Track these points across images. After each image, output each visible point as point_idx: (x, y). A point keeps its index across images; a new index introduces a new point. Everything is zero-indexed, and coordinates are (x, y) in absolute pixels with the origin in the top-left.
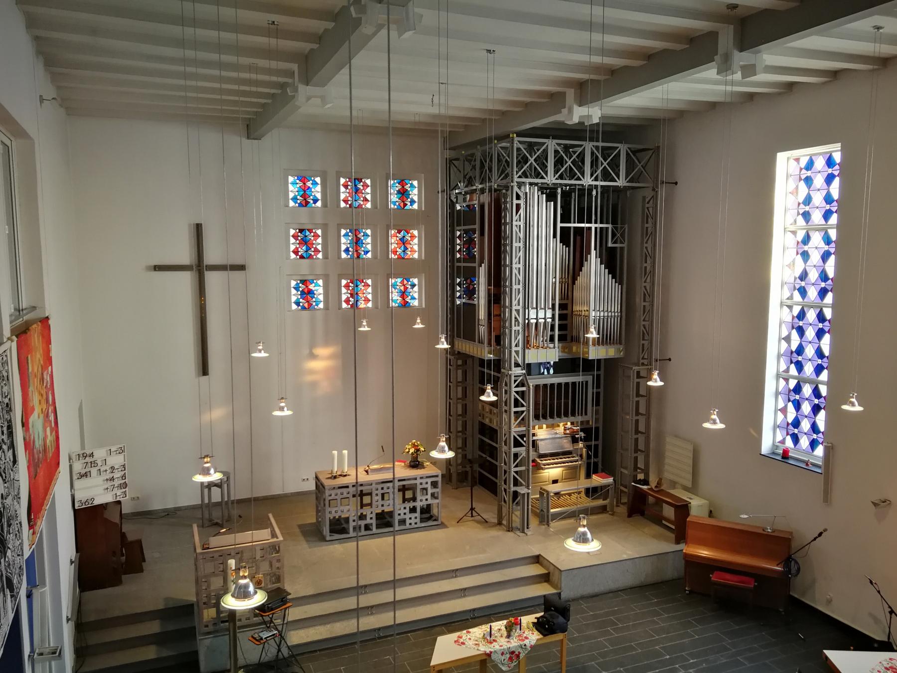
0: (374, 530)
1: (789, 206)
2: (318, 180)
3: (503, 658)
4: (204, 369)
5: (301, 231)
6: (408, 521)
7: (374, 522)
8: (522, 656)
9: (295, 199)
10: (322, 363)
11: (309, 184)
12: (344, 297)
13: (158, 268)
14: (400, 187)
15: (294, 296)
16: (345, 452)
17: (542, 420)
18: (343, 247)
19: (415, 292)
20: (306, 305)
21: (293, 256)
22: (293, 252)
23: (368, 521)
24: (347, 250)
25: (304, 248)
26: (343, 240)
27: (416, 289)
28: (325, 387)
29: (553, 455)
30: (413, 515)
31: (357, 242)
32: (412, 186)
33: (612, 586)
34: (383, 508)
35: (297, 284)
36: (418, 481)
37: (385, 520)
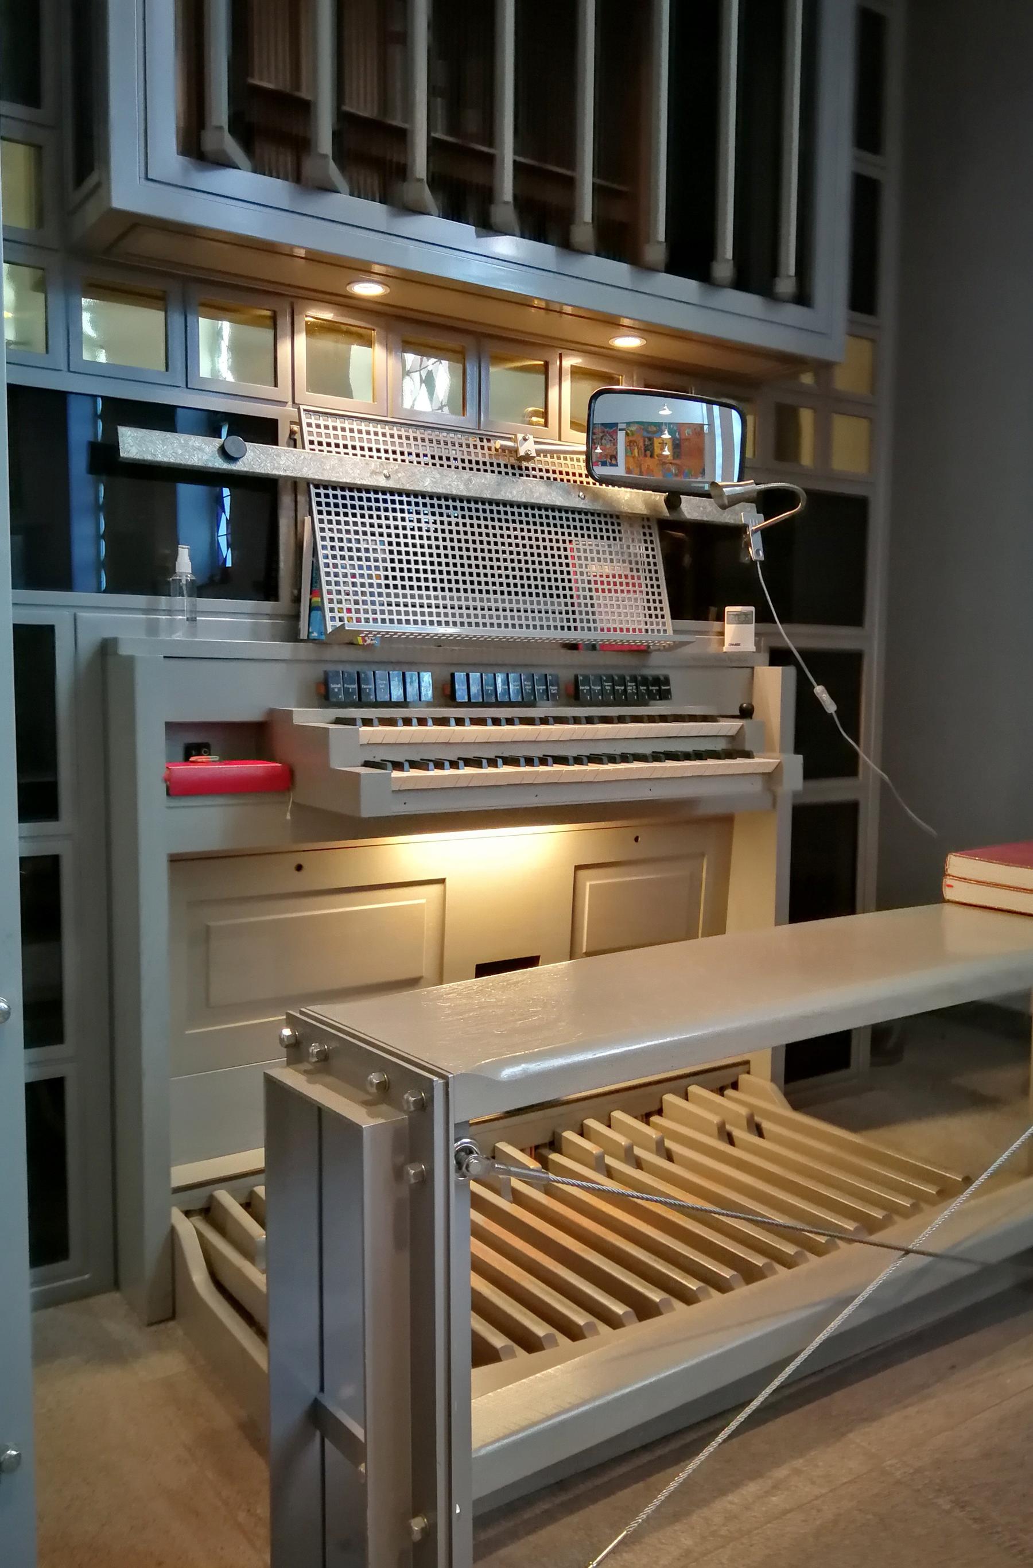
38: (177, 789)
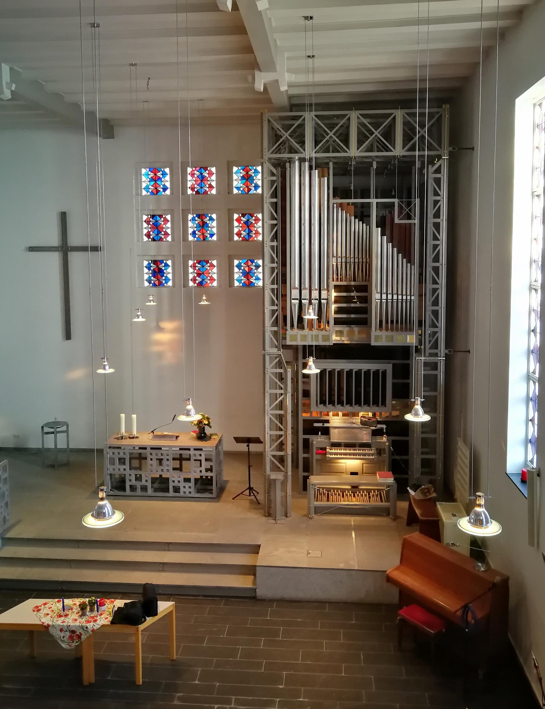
0: (150, 491)
1: (536, 165)
2: (167, 170)
3: (62, 634)
4: (68, 336)
5: (153, 216)
6: (182, 490)
7: (149, 484)
8: (83, 637)
9: (147, 188)
10: (167, 336)
11: (159, 174)
12: (191, 276)
13: (32, 249)
14: (244, 173)
15: (146, 274)
16: (134, 416)
18: (190, 231)
20: (157, 283)
21: (146, 239)
22: (237, 234)
23: (143, 483)
24: (194, 233)
25: (156, 232)
26: (190, 224)
27: (260, 270)
28: (169, 358)
29: (348, 445)
30: (187, 485)
31: (203, 225)
32: (256, 172)
33: (321, 595)
34: (161, 473)
35: (149, 264)
36: (192, 452)
37: (162, 485)
38: (316, 454)
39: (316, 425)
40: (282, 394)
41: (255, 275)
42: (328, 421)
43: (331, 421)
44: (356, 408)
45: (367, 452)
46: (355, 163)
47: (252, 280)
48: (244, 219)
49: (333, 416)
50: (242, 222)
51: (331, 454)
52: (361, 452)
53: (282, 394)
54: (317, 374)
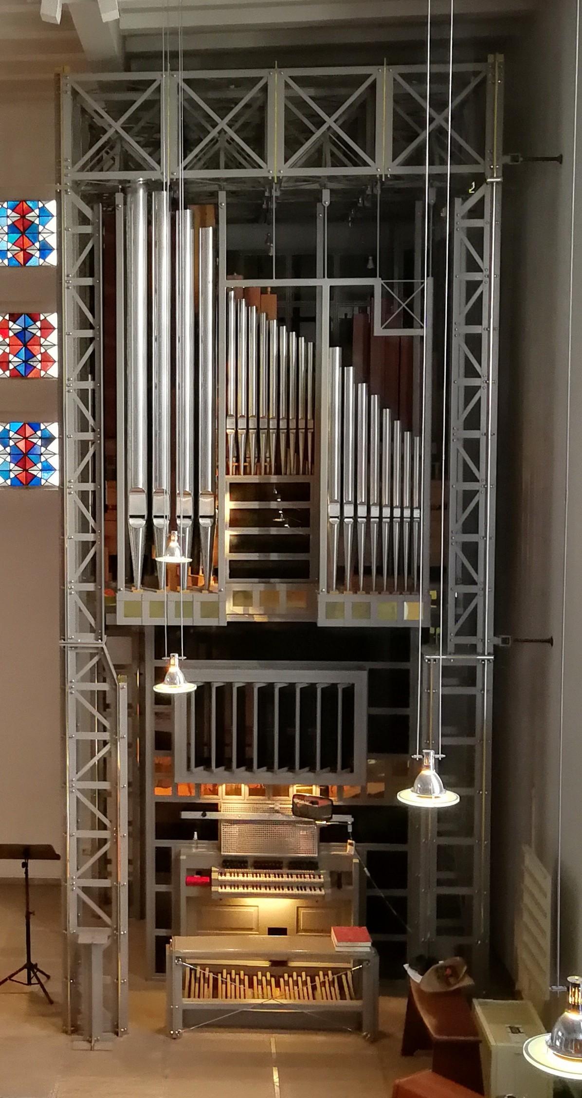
14: (15, 216)
17: (242, 772)
19: (52, 454)
27: (54, 446)
29: (262, 864)
32: (44, 214)
39: (186, 815)
40: (105, 743)
41: (43, 459)
42: (214, 807)
43: (222, 807)
44: (282, 776)
45: (308, 880)
46: (278, 194)
47: (35, 471)
48: (15, 326)
49: (227, 794)
50: (11, 334)
51: (223, 884)
52: (295, 879)
53: (105, 743)
54: (189, 695)
